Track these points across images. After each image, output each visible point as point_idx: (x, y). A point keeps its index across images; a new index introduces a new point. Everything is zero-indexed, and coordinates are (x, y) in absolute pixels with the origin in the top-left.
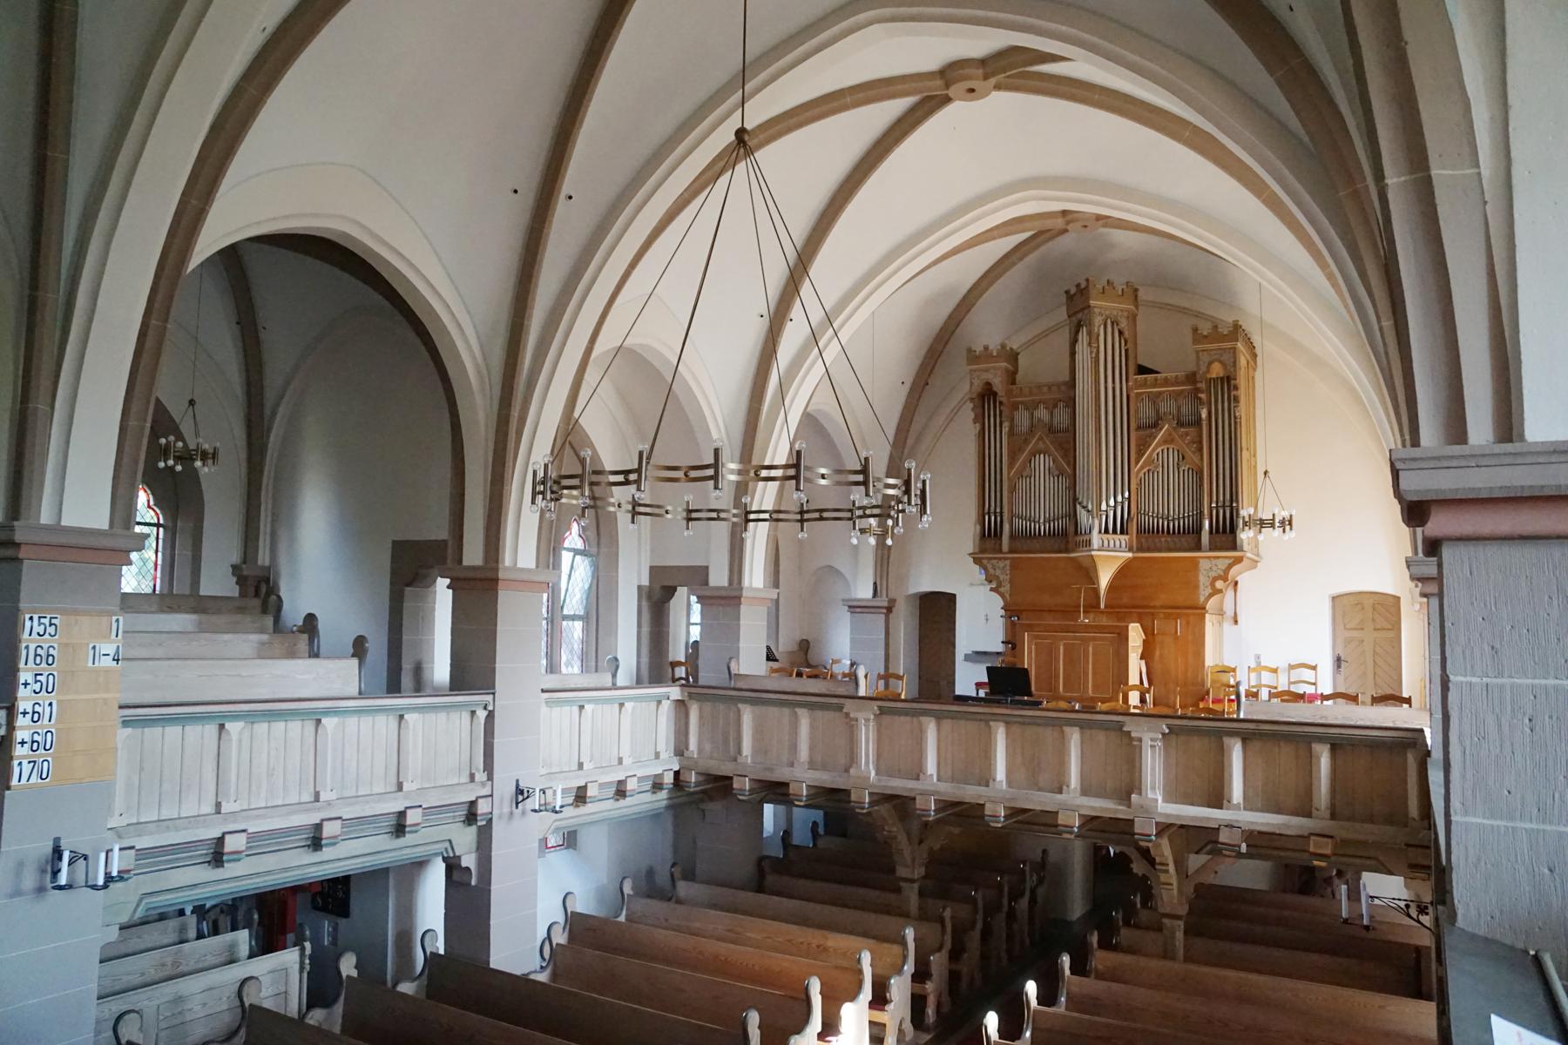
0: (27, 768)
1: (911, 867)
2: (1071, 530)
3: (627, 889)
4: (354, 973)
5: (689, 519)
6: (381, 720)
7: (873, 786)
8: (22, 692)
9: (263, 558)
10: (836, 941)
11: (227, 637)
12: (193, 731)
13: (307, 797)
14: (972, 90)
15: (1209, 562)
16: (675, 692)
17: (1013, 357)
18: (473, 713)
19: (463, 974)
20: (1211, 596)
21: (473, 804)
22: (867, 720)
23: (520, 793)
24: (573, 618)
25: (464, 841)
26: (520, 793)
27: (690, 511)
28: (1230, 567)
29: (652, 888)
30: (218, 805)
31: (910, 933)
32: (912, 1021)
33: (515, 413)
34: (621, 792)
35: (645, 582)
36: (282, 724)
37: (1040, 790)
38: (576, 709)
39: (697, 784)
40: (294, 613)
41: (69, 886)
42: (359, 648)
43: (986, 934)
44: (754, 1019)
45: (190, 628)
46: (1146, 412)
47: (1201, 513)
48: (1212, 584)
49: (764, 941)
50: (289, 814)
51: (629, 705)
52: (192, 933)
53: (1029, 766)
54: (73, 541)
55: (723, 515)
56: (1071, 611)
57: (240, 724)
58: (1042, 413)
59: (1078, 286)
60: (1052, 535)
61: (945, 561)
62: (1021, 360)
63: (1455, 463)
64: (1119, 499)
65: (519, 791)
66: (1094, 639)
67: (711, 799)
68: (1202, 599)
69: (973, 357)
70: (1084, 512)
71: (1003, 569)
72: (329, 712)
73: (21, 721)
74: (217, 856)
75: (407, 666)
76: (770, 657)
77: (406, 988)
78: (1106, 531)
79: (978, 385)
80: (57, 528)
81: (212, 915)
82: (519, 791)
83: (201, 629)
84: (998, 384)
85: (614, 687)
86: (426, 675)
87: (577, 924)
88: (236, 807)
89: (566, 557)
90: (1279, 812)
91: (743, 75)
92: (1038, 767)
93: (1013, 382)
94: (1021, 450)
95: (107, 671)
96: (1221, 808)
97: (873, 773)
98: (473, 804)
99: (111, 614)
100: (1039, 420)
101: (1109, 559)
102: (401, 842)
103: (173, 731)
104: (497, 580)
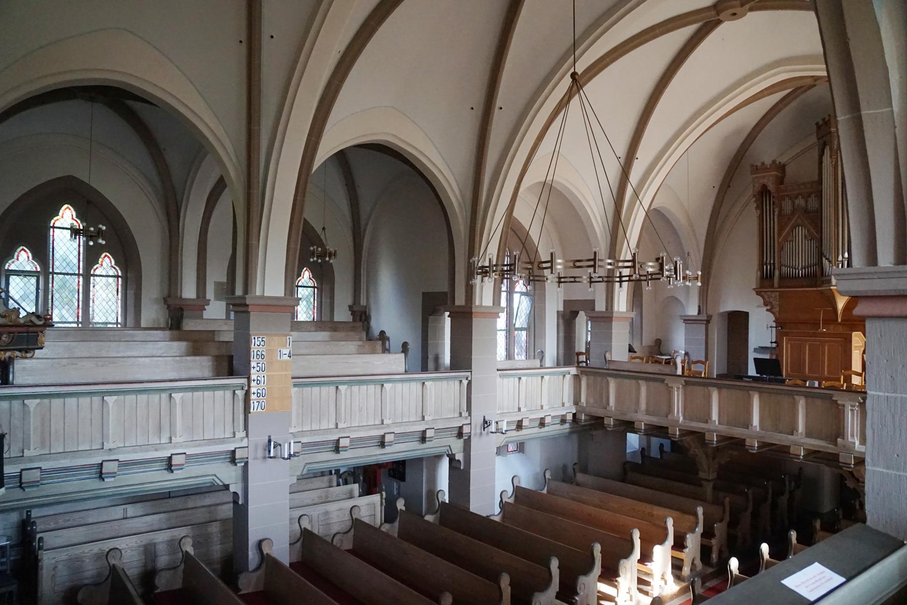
0: (256, 404)
1: (707, 472)
2: (819, 273)
3: (548, 476)
4: (404, 508)
5: (560, 282)
6: (413, 384)
7: (681, 425)
8: (253, 371)
9: (363, 302)
10: (658, 511)
11: (343, 343)
12: (325, 389)
13: (378, 422)
14: (735, 14)
16: (573, 370)
17: (782, 168)
18: (461, 381)
19: (457, 513)
21: (461, 428)
22: (678, 388)
23: (486, 423)
24: (521, 329)
25: (457, 447)
26: (486, 423)
27: (560, 278)
29: (565, 475)
30: (337, 424)
31: (700, 511)
32: (701, 560)
33: (479, 226)
34: (542, 424)
35: (561, 309)
36: (365, 387)
37: (781, 432)
38: (517, 379)
39: (585, 420)
40: (376, 330)
41: (274, 457)
42: (405, 348)
43: (755, 515)
44: (597, 548)
45: (327, 339)
49: (616, 508)
50: (370, 430)
52: (335, 484)
53: (771, 418)
54: (269, 302)
55: (577, 280)
56: (816, 325)
57: (346, 387)
58: (800, 202)
59: (823, 119)
60: (806, 277)
61: (739, 295)
62: (788, 169)
63: (849, 277)
65: (485, 422)
67: (595, 429)
69: (755, 169)
70: (827, 262)
71: (774, 296)
72: (388, 381)
73: (253, 384)
74: (337, 449)
75: (431, 357)
76: (631, 350)
77: (429, 518)
79: (758, 187)
80: (262, 297)
81: (344, 477)
82: (485, 422)
83: (333, 339)
84: (771, 187)
85: (542, 367)
86: (441, 361)
87: (519, 491)
88: (344, 426)
89: (516, 297)
91: (575, 46)
92: (779, 419)
93: (782, 183)
95: (286, 362)
97: (681, 419)
98: (461, 428)
99: (286, 336)
102: (424, 446)
103: (316, 389)
104: (471, 313)
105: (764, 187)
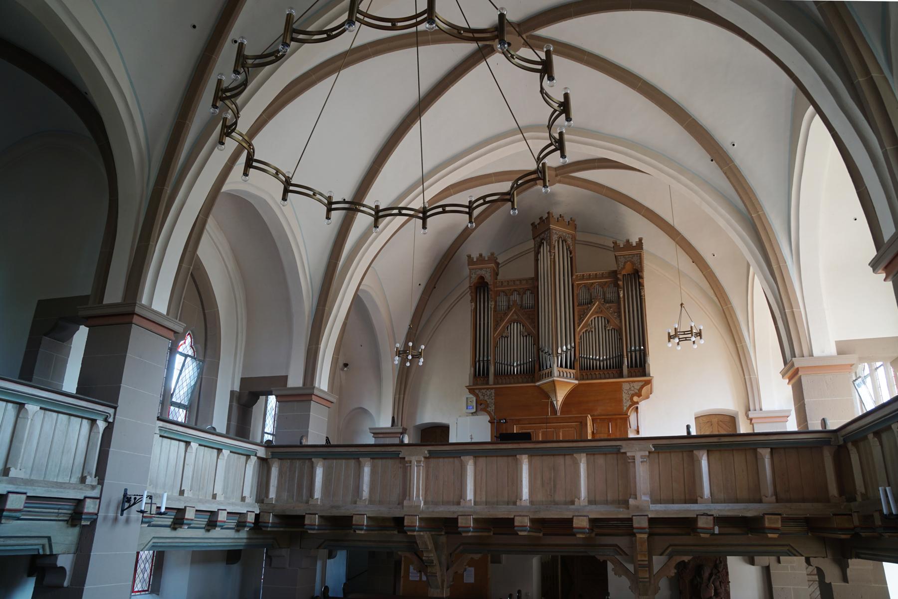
7: (422, 512)
15: (628, 384)
18: (93, 422)
20: (630, 406)
21: (80, 503)
22: (419, 462)
23: (127, 501)
24: (179, 406)
26: (127, 501)
28: (642, 387)
33: (168, 190)
35: (237, 388)
46: (583, 295)
47: (622, 356)
48: (631, 399)
51: (226, 452)
58: (515, 297)
64: (569, 347)
65: (126, 499)
66: (563, 427)
68: (625, 408)
71: (489, 397)
78: (561, 366)
82: (126, 499)
84: (488, 278)
89: (179, 359)
90: (737, 501)
94: (502, 320)
96: (696, 502)
100: (515, 301)
101: (563, 385)
105: (482, 278)
